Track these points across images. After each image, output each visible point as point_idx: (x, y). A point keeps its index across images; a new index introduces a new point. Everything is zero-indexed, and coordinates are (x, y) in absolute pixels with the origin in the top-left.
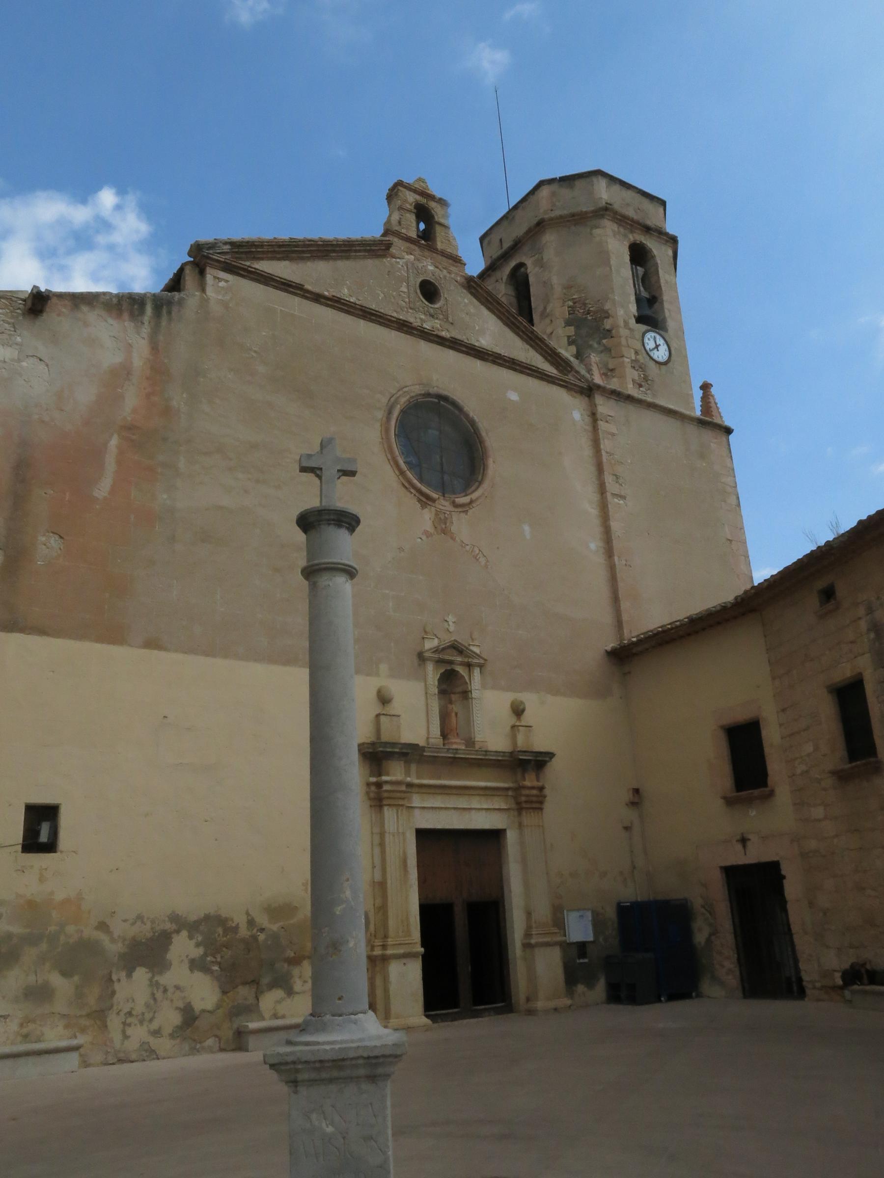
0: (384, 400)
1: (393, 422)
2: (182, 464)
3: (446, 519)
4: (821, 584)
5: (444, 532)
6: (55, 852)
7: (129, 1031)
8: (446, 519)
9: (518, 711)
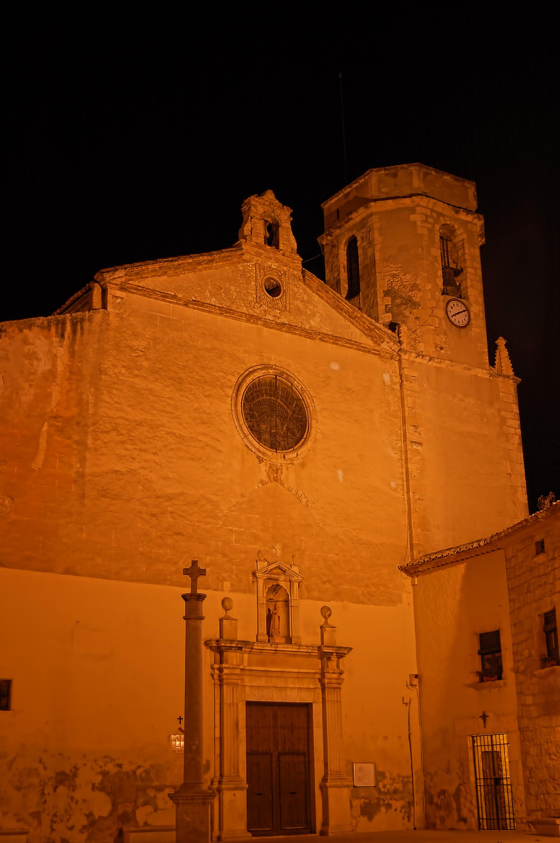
0: (234, 380)
1: (240, 398)
2: (89, 441)
3: (277, 470)
5: (276, 479)
6: (10, 710)
7: (55, 826)
8: (277, 470)
9: (326, 612)
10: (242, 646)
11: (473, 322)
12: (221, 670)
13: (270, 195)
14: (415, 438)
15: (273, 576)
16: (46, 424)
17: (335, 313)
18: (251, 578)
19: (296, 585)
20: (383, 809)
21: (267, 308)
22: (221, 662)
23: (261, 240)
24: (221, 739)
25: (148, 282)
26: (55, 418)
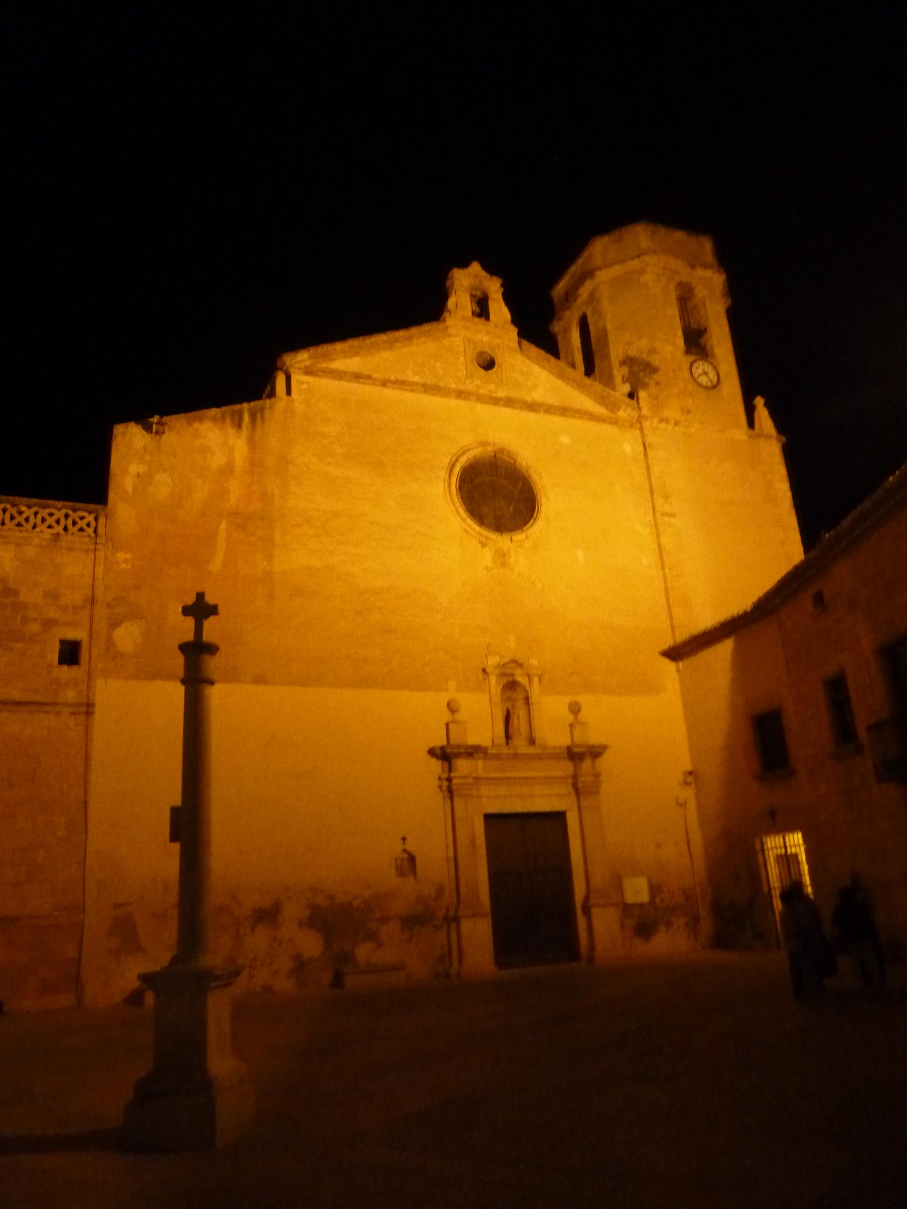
4: (813, 590)
5: (503, 565)
9: (575, 709)
10: (473, 752)
11: (723, 381)
12: (449, 780)
13: (475, 267)
14: (667, 509)
15: (507, 671)
16: (224, 522)
17: (559, 383)
18: (481, 674)
19: (536, 680)
20: (662, 928)
21: (480, 382)
22: (450, 770)
23: (469, 313)
24: (456, 858)
25: (338, 364)
26: (235, 514)
